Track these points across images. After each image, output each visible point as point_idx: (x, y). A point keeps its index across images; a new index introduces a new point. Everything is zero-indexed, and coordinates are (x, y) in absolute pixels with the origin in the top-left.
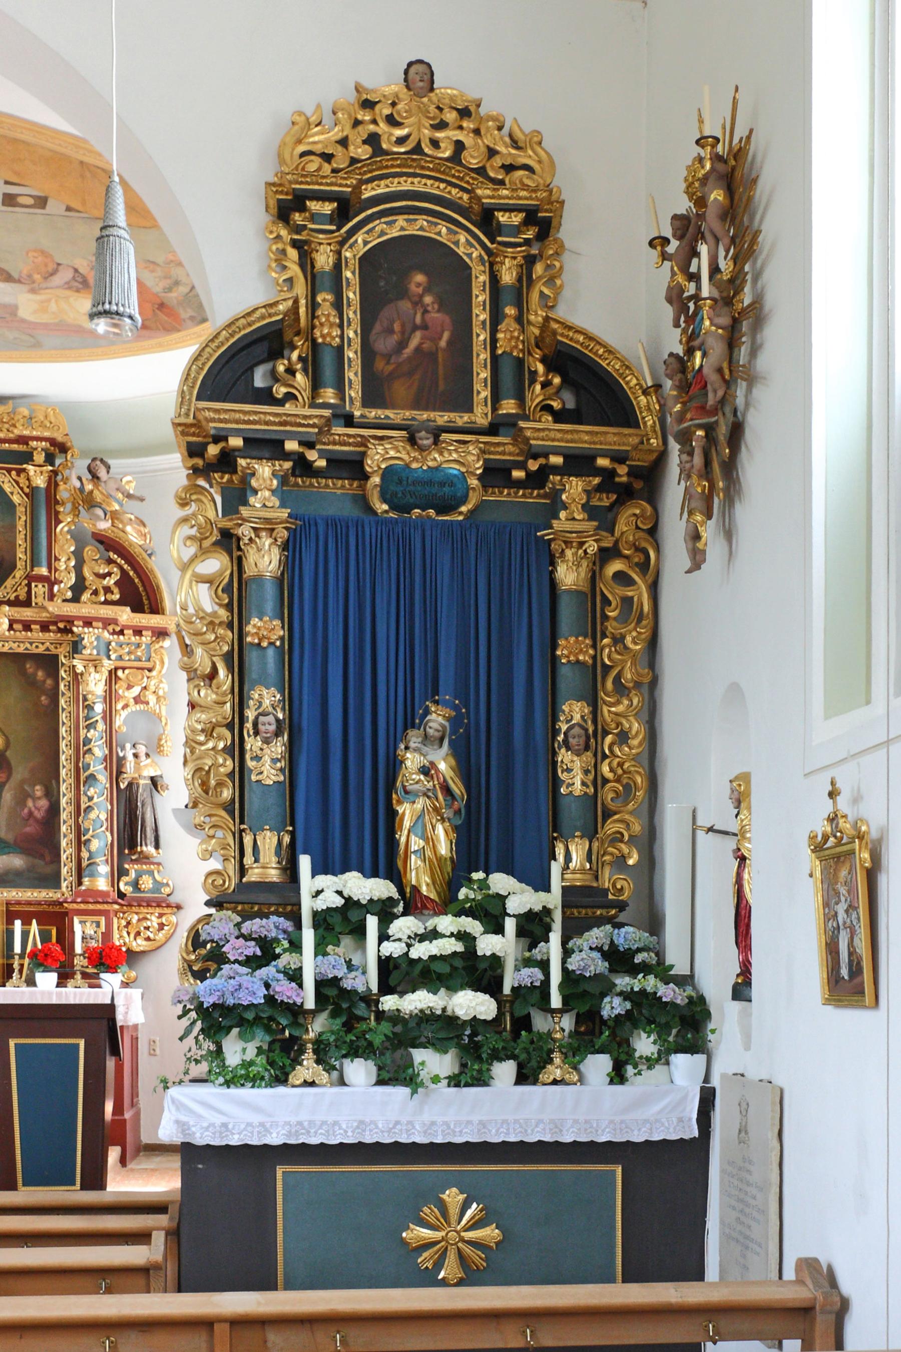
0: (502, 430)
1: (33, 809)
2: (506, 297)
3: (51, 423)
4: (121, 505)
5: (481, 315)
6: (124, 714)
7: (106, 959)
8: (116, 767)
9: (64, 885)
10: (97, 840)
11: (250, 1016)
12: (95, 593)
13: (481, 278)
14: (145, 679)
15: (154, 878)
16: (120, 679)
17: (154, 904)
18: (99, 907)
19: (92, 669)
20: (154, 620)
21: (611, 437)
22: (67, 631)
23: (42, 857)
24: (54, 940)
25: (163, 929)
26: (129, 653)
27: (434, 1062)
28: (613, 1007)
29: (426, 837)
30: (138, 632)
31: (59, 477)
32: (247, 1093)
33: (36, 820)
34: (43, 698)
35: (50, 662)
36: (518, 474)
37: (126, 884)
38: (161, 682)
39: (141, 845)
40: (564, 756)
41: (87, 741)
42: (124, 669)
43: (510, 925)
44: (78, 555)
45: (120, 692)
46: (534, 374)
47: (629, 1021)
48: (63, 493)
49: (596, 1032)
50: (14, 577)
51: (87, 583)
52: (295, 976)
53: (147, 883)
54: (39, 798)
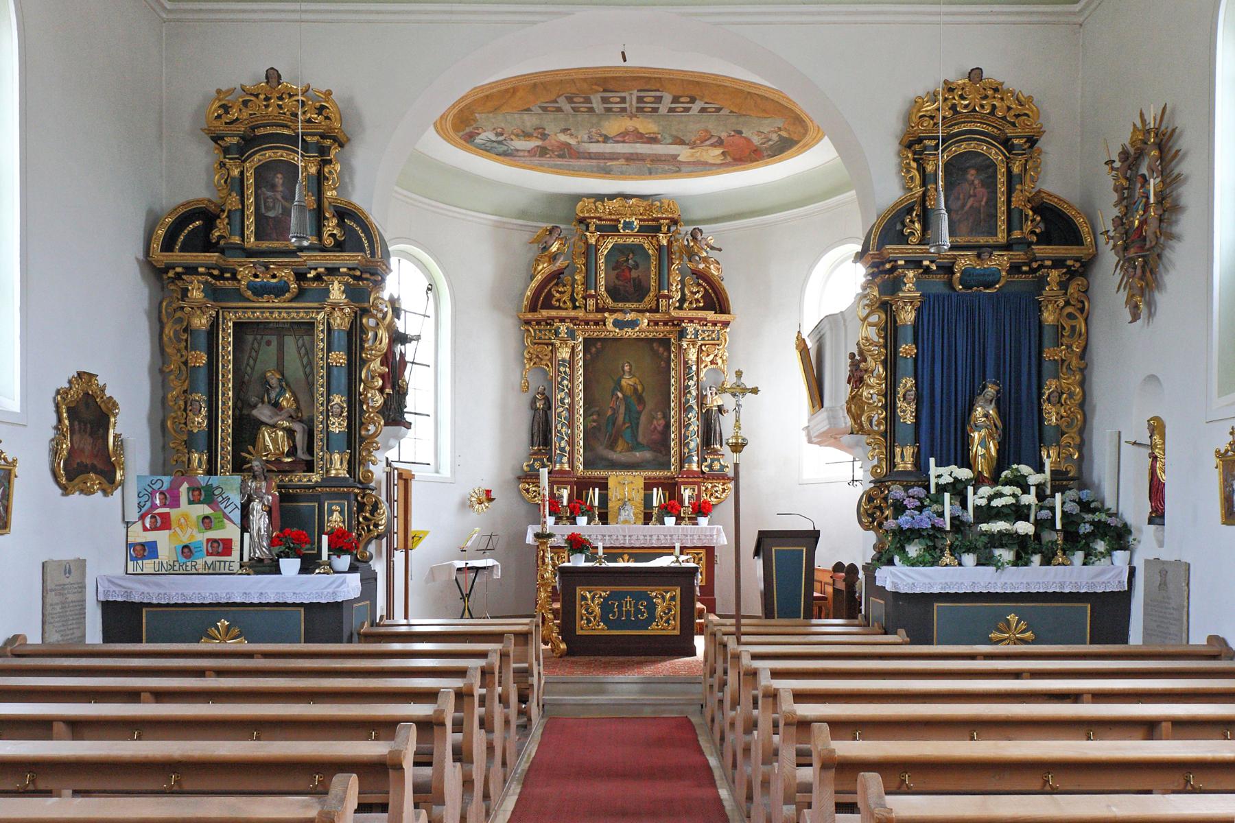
0: (1015, 247)
2: (1015, 180)
5: (1001, 188)
7: (702, 509)
8: (701, 399)
11: (925, 533)
12: (691, 303)
13: (1002, 170)
20: (724, 317)
21: (1073, 251)
27: (1006, 555)
28: (1085, 529)
29: (983, 446)
30: (715, 324)
32: (921, 569)
35: (665, 343)
36: (1025, 268)
40: (1046, 406)
43: (1033, 490)
46: (1027, 216)
47: (1092, 536)
48: (675, 248)
49: (1074, 540)
52: (941, 515)
53: (717, 466)
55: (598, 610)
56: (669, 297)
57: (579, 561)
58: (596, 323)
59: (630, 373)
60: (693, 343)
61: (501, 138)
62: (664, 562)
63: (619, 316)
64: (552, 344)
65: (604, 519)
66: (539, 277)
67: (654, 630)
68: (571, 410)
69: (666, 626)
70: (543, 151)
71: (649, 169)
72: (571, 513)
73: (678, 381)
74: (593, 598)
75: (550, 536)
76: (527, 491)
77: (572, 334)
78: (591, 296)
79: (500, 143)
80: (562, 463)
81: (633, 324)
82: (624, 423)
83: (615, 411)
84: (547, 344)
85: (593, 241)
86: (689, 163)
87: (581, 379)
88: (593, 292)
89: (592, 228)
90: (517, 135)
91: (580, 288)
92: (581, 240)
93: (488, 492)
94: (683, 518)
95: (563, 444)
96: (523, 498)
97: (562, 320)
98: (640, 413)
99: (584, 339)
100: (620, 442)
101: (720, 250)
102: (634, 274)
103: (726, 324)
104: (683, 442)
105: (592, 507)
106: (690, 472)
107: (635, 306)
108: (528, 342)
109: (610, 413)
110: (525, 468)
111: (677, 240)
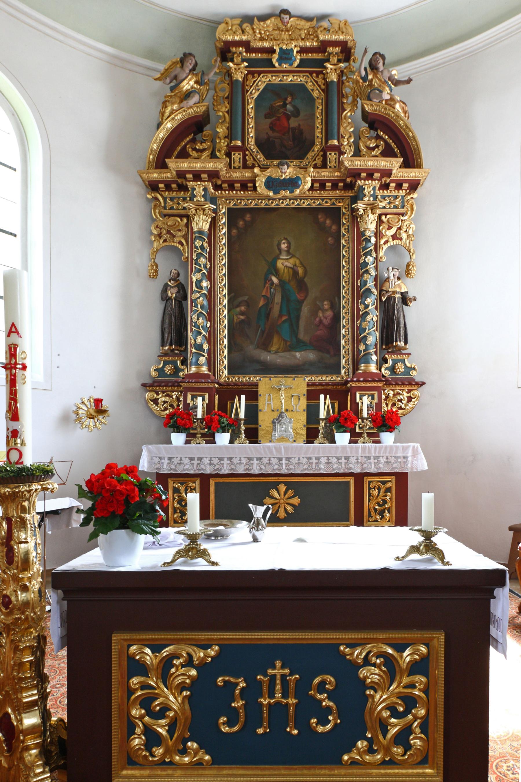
1: (322, 318)
6: (385, 247)
7: (386, 422)
8: (381, 282)
9: (343, 371)
10: (371, 337)
14: (400, 221)
15: (405, 365)
16: (383, 222)
18: (375, 384)
19: (370, 211)
20: (412, 174)
23: (328, 352)
24: (349, 409)
25: (411, 401)
26: (390, 203)
31: (344, 78)
33: (324, 326)
34: (330, 239)
35: (334, 213)
38: (411, 223)
39: (396, 341)
41: (366, 264)
42: (386, 215)
45: (383, 231)
48: (347, 90)
50: (313, 151)
54: (327, 310)
58: (244, 186)
59: (288, 252)
60: (373, 208)
63: (272, 172)
65: (253, 436)
66: (169, 125)
68: (211, 296)
76: (156, 401)
78: (237, 149)
80: (198, 364)
81: (292, 183)
82: (280, 316)
83: (269, 301)
84: (181, 216)
85: (239, 77)
87: (225, 260)
88: (239, 143)
89: (237, 60)
93: (98, 401)
94: (360, 435)
95: (199, 340)
96: (151, 410)
99: (229, 210)
100: (275, 340)
102: (293, 123)
103: (414, 186)
104: (359, 337)
105: (237, 420)
106: (367, 374)
109: (261, 303)
110: (154, 374)
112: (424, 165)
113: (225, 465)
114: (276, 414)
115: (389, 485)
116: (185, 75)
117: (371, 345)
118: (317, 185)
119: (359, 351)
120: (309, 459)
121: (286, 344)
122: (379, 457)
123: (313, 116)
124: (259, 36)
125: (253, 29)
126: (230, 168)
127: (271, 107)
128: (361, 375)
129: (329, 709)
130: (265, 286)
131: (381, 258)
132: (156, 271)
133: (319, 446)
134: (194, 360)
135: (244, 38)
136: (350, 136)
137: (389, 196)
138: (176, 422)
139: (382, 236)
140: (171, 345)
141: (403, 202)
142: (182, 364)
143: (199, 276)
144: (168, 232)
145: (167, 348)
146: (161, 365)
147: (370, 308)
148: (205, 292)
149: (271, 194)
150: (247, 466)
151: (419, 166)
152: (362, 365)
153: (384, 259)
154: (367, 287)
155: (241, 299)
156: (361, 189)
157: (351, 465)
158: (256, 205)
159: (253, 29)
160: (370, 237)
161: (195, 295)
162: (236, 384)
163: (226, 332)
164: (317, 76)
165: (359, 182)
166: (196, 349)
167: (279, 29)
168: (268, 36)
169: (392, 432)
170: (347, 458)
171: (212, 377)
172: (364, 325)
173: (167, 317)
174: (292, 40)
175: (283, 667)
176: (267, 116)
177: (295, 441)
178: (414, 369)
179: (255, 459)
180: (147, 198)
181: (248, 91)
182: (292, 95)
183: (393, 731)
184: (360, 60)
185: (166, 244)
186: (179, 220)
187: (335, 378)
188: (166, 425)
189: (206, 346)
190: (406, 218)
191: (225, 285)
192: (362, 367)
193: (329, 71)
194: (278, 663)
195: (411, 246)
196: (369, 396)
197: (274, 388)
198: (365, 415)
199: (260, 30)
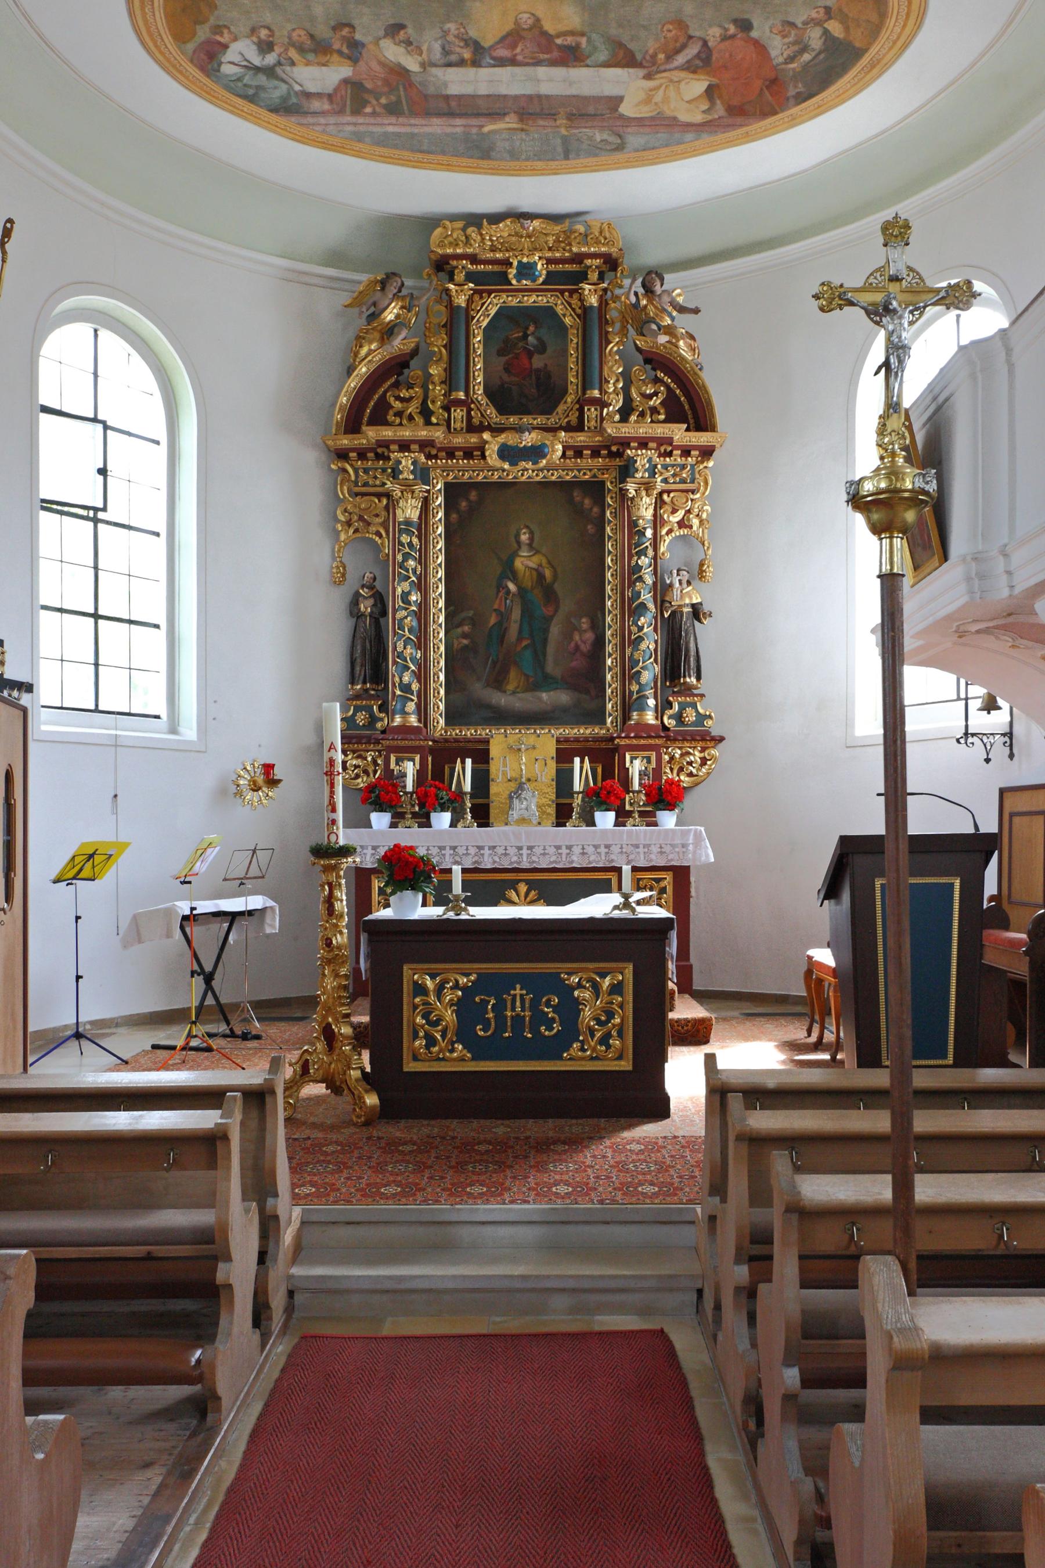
1: (579, 642)
3: (605, 239)
4: (673, 319)
6: (668, 539)
7: (664, 796)
8: (662, 591)
9: (609, 720)
14: (690, 502)
15: (697, 711)
17: (698, 738)
19: (644, 493)
20: (703, 438)
22: (619, 454)
23: (587, 692)
26: (674, 475)
30: (686, 452)
33: (583, 654)
34: (589, 527)
35: (595, 489)
37: (669, 718)
38: (705, 504)
39: (685, 677)
42: (669, 492)
44: (626, 376)
45: (665, 517)
48: (613, 314)
50: (566, 402)
51: (634, 404)
53: (690, 716)
54: (585, 631)
55: (450, 1016)
56: (602, 404)
57: (417, 909)
58: (468, 454)
60: (648, 487)
61: (271, 59)
62: (597, 906)
63: (509, 438)
64: (388, 495)
65: (482, 816)
67: (576, 1059)
68: (422, 614)
69: (598, 1052)
70: (354, 97)
71: (565, 140)
72: (422, 805)
73: (619, 559)
74: (440, 990)
75: (346, 851)
77: (423, 475)
78: (458, 403)
79: (269, 72)
80: (404, 713)
81: (536, 453)
82: (520, 639)
83: (504, 617)
84: (379, 496)
85: (461, 301)
86: (640, 122)
87: (441, 559)
88: (461, 395)
89: (460, 277)
90: (301, 50)
91: (438, 390)
92: (439, 301)
93: (268, 768)
94: (629, 814)
95: (407, 678)
97: (404, 446)
98: (548, 620)
99: (448, 486)
100: (513, 674)
101: (696, 311)
102: (538, 362)
103: (707, 452)
104: (629, 673)
105: (460, 794)
106: (642, 728)
107: (540, 420)
108: (343, 492)
109: (493, 620)
111: (616, 298)
112: (719, 427)
113: (447, 857)
114: (513, 786)
115: (663, 884)
116: (386, 303)
117: (647, 684)
118: (570, 453)
119: (631, 693)
120: (558, 847)
121: (528, 680)
122: (649, 845)
123: (565, 352)
124: (489, 243)
125: (481, 235)
126: (450, 431)
127: (506, 341)
128: (632, 728)
129: (553, 1020)
130: (497, 594)
131: (663, 554)
132: (343, 575)
133: (573, 832)
134: (399, 707)
135: (470, 251)
136: (617, 380)
137: (673, 466)
138: (378, 796)
139: (663, 523)
140: (364, 682)
141: (693, 474)
142: (380, 711)
143: (406, 586)
144: (361, 518)
145: (359, 687)
146: (351, 712)
147: (645, 630)
148: (415, 608)
149: (506, 466)
150: (476, 858)
151: (713, 429)
152: (635, 713)
153: (668, 555)
154: (640, 600)
155: (464, 615)
156: (632, 461)
157: (613, 857)
158: (485, 478)
159: (481, 235)
160: (645, 529)
161: (401, 614)
162: (456, 741)
163: (442, 663)
164: (571, 296)
165: (629, 452)
166: (401, 691)
167: (517, 234)
168: (502, 244)
169: (672, 810)
170: (607, 847)
171: (424, 733)
172: (636, 656)
173: (359, 642)
174: (536, 249)
175: (521, 989)
176: (501, 353)
177: (539, 823)
178: (710, 717)
179: (486, 848)
180: (332, 470)
181: (473, 318)
182: (535, 323)
183: (598, 1035)
184: (672, 66)
185: (358, 535)
186: (377, 501)
187: (598, 731)
188: (364, 801)
189: (415, 687)
190: (698, 496)
191: (440, 595)
192: (635, 715)
193: (586, 292)
194: (518, 986)
195: (706, 537)
196: (643, 758)
197: (511, 748)
198: (636, 786)
199: (491, 236)
